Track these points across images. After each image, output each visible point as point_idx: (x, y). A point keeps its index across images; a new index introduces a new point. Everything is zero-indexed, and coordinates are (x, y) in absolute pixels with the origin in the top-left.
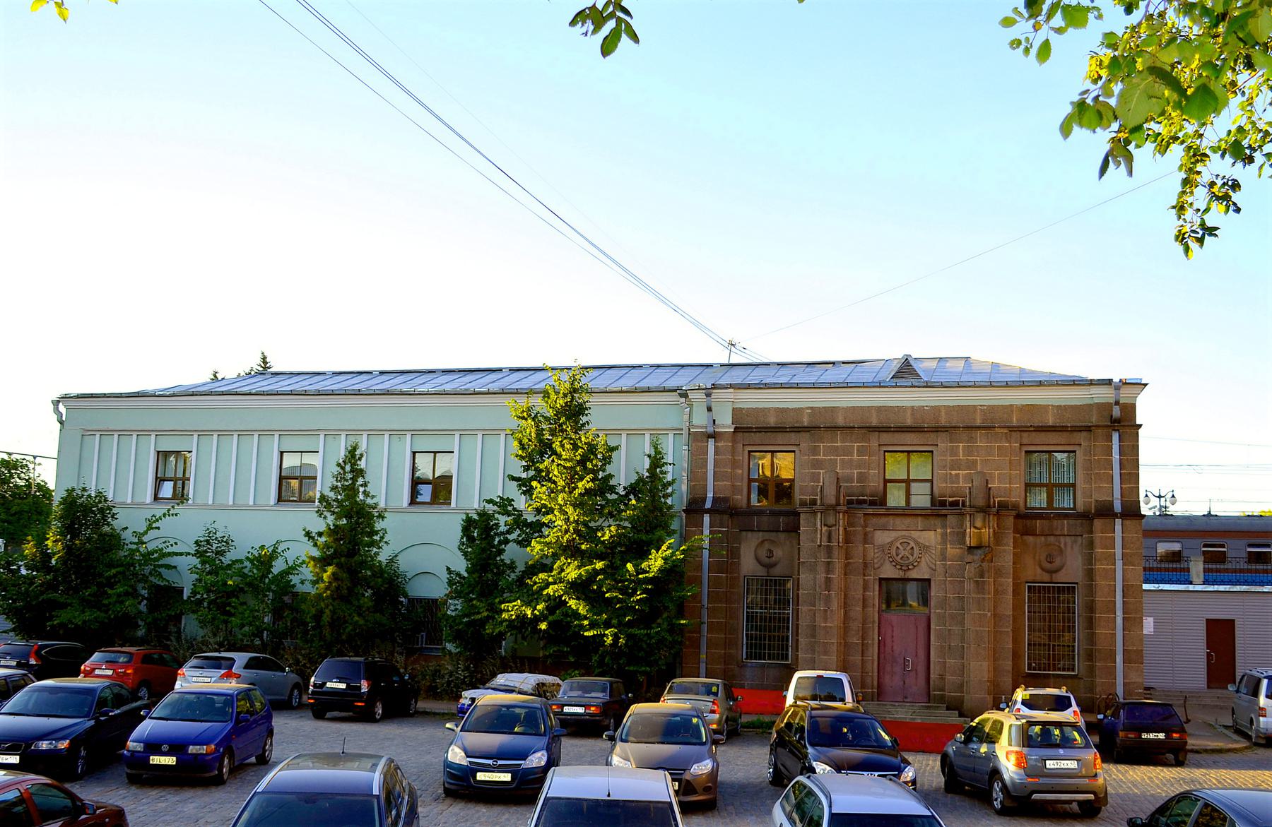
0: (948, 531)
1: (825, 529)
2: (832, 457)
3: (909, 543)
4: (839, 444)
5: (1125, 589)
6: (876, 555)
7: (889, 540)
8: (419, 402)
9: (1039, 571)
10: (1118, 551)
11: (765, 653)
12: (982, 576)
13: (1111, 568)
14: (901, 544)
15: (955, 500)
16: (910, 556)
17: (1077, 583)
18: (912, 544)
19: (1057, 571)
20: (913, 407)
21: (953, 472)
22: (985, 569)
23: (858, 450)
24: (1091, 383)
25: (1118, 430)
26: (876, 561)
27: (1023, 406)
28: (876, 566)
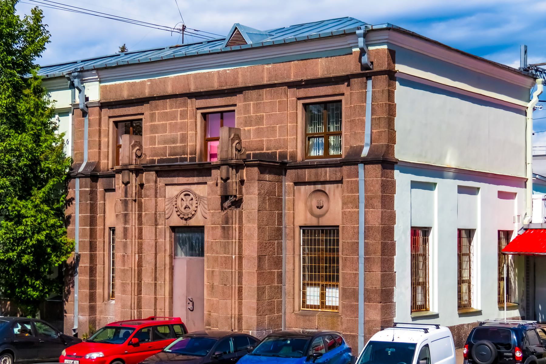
2: (164, 122)
3: (189, 195)
4: (168, 110)
6: (166, 207)
7: (176, 193)
8: (131, 73)
9: (309, 215)
10: (362, 194)
12: (227, 223)
13: (355, 211)
16: (190, 206)
18: (192, 196)
21: (246, 128)
22: (229, 216)
23: (180, 115)
26: (167, 212)
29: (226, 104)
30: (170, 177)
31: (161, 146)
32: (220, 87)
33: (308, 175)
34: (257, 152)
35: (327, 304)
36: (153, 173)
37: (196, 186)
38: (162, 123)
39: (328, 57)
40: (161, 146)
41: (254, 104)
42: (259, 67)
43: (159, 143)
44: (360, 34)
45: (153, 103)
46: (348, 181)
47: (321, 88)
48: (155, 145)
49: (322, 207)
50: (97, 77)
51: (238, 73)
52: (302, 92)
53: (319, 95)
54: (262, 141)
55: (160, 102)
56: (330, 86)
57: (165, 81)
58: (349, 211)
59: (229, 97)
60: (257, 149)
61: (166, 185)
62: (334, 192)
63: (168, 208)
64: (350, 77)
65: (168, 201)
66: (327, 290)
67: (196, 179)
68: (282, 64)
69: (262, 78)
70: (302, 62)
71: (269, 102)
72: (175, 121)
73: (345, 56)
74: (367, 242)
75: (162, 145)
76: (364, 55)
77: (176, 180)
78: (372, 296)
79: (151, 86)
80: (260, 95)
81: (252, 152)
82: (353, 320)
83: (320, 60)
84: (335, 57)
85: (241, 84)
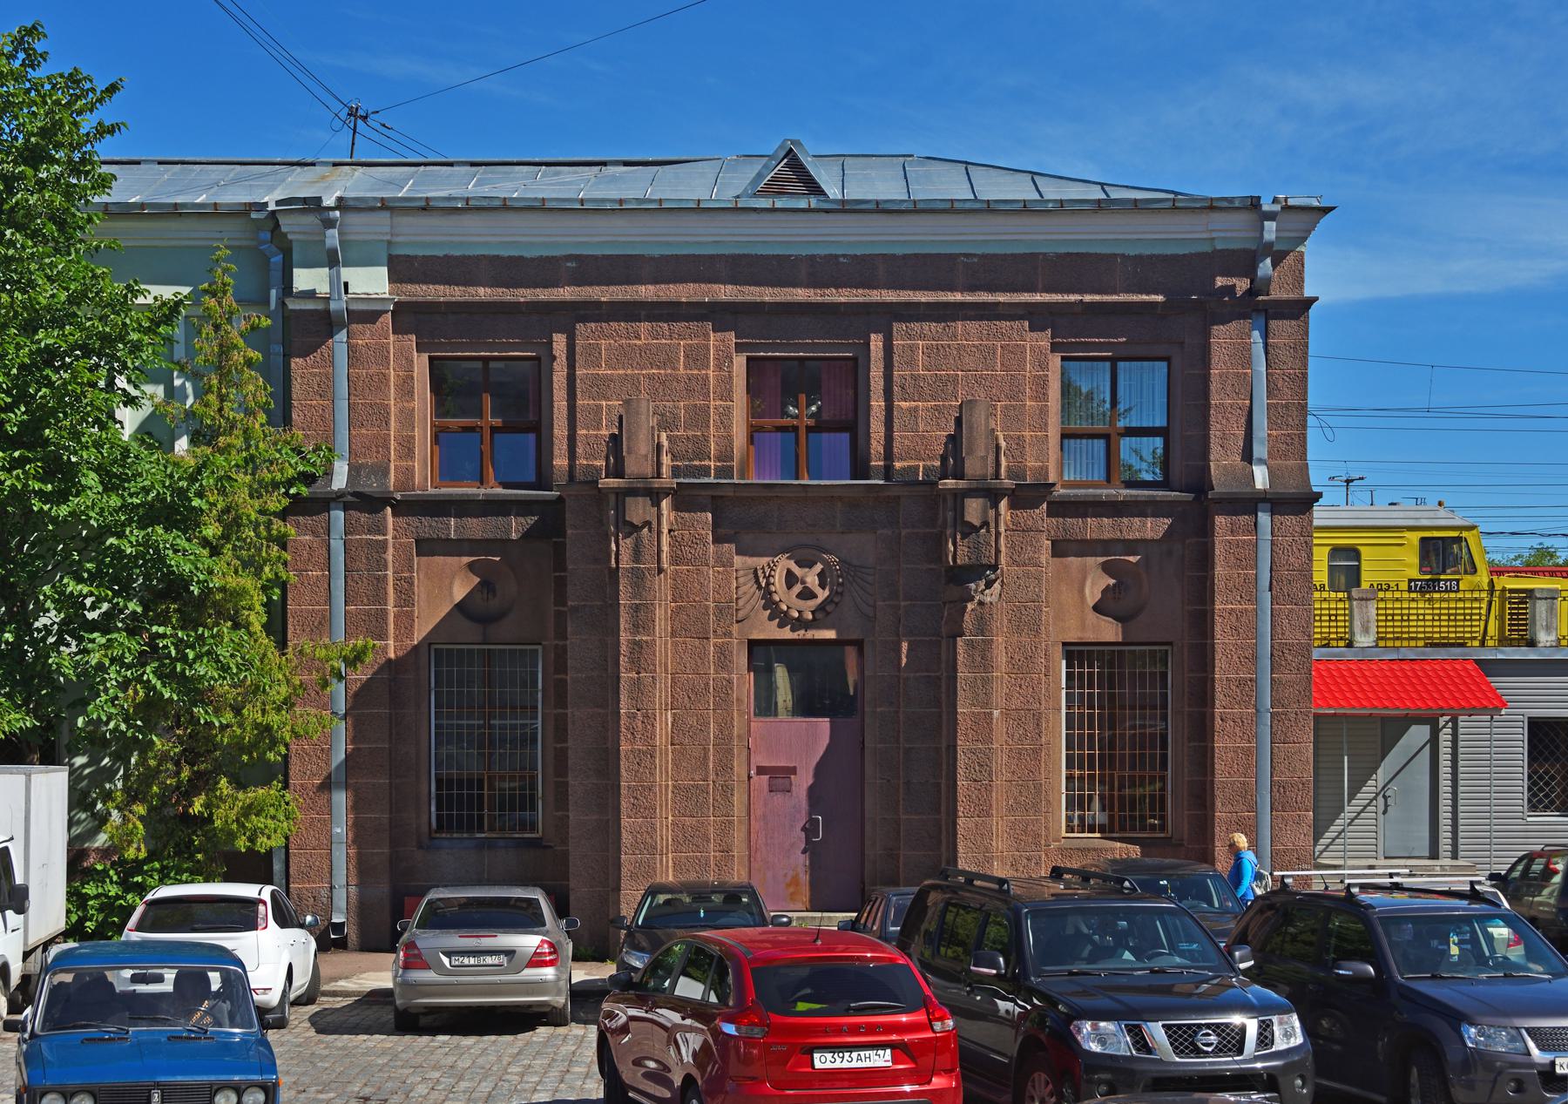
0: (904, 532)
11: (481, 817)
15: (909, 467)
17: (1170, 644)
20: (812, 257)
23: (687, 356)
24: (1211, 206)
25: (1167, 359)
27: (1059, 256)
28: (741, 614)
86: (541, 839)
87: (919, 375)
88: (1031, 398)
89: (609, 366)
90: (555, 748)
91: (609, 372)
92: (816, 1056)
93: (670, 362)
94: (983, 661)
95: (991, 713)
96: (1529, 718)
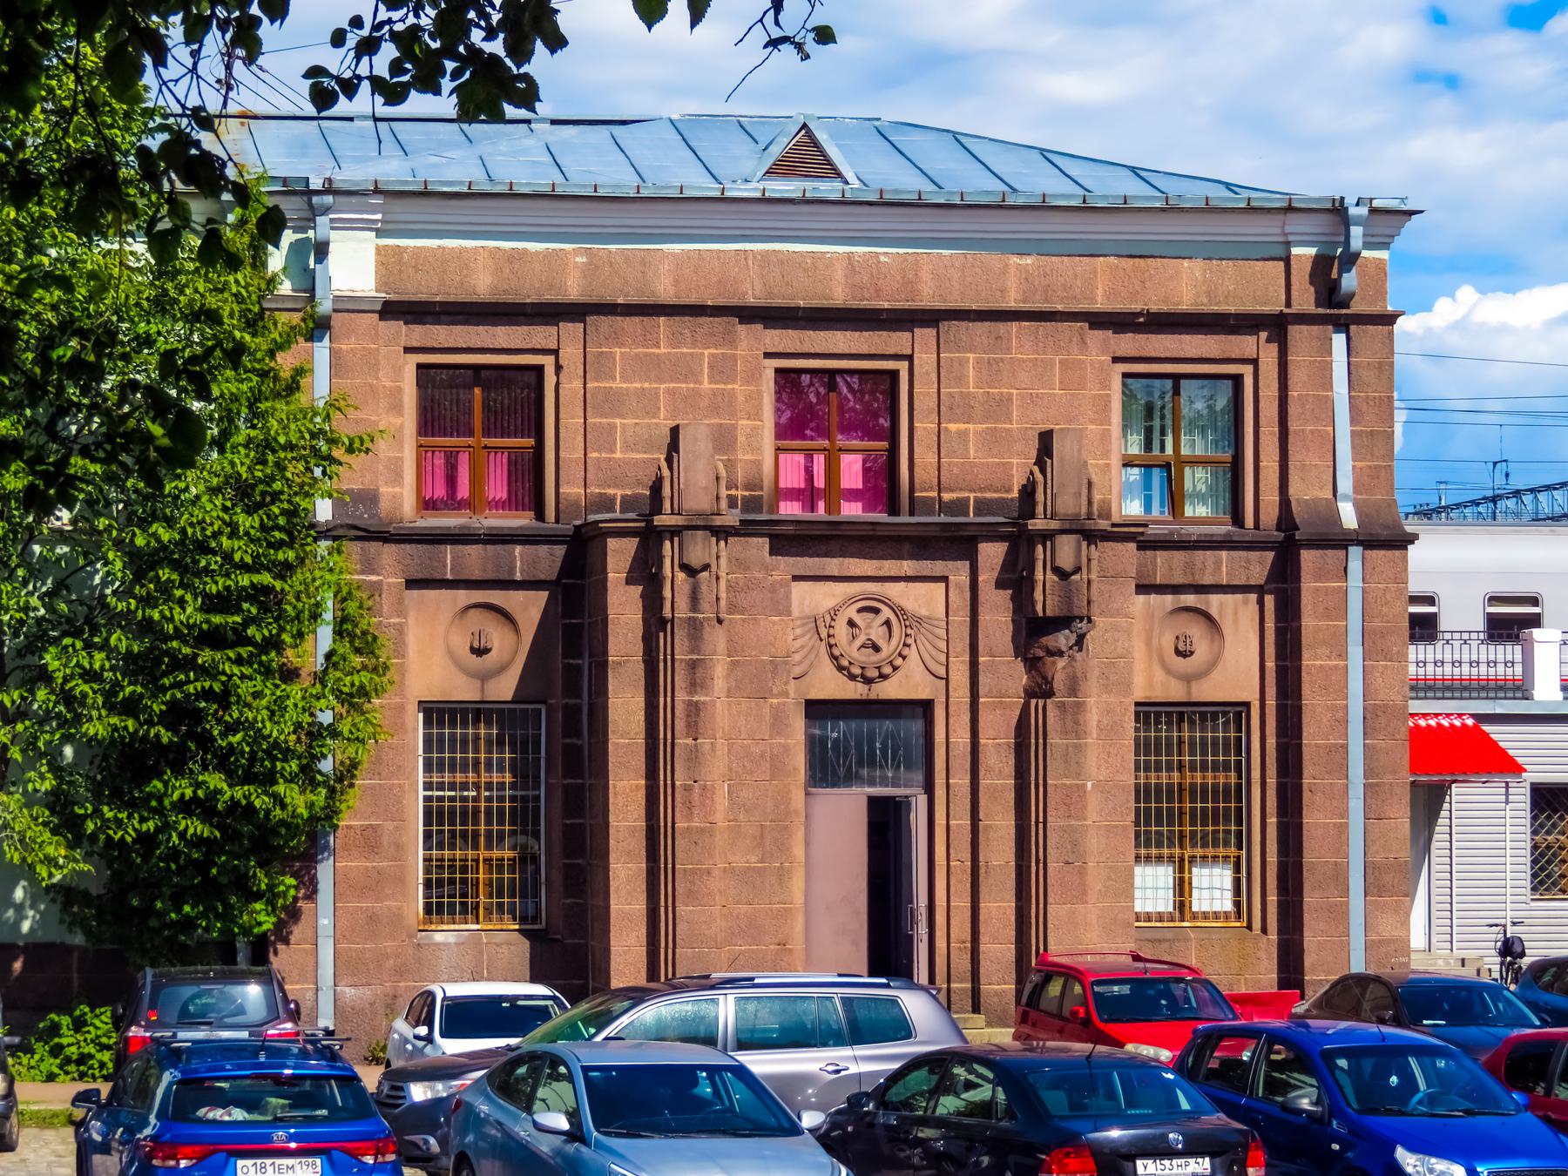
1: (681, 576)
2: (646, 385)
4: (663, 350)
5: (1368, 716)
7: (829, 603)
8: (422, 218)
9: (1159, 675)
13: (1336, 666)
14: (860, 611)
15: (958, 499)
18: (886, 613)
19: (1202, 674)
23: (711, 367)
28: (797, 671)
29: (873, 352)
30: (811, 556)
31: (634, 456)
32: (854, 298)
33: (1166, 566)
34: (989, 495)
35: (1195, 908)
36: (764, 542)
37: (902, 585)
38: (638, 385)
39: (1209, 259)
40: (634, 456)
41: (978, 362)
42: (993, 259)
43: (627, 447)
44: (1359, 217)
45: (604, 323)
46: (1317, 589)
47: (1187, 338)
48: (612, 451)
49: (487, 651)
50: (379, 216)
51: (917, 268)
52: (1129, 343)
53: (1182, 355)
54: (1008, 466)
55: (632, 324)
56: (1216, 337)
57: (644, 261)
58: (1321, 666)
59: (885, 333)
60: (989, 488)
61: (796, 578)
62: (1236, 613)
63: (802, 647)
64: (1290, 319)
65: (803, 625)
66: (1195, 870)
67: (907, 567)
68: (1066, 259)
69: (1003, 291)
70: (1131, 261)
71: (1031, 360)
72: (692, 386)
73: (1260, 263)
74: (1372, 745)
75: (638, 452)
76: (1349, 271)
77: (833, 565)
78: (1388, 878)
79: (591, 270)
80: (998, 338)
81: (972, 495)
82: (1334, 943)
83: (1186, 263)
84: (1230, 263)
85: (928, 299)
86: (545, 930)
87: (969, 393)
88: (1092, 422)
89: (624, 379)
90: (565, 825)
91: (624, 385)
92: (1139, 1163)
93: (691, 375)
94: (1076, 729)
95: (1084, 786)
96: (1532, 784)
